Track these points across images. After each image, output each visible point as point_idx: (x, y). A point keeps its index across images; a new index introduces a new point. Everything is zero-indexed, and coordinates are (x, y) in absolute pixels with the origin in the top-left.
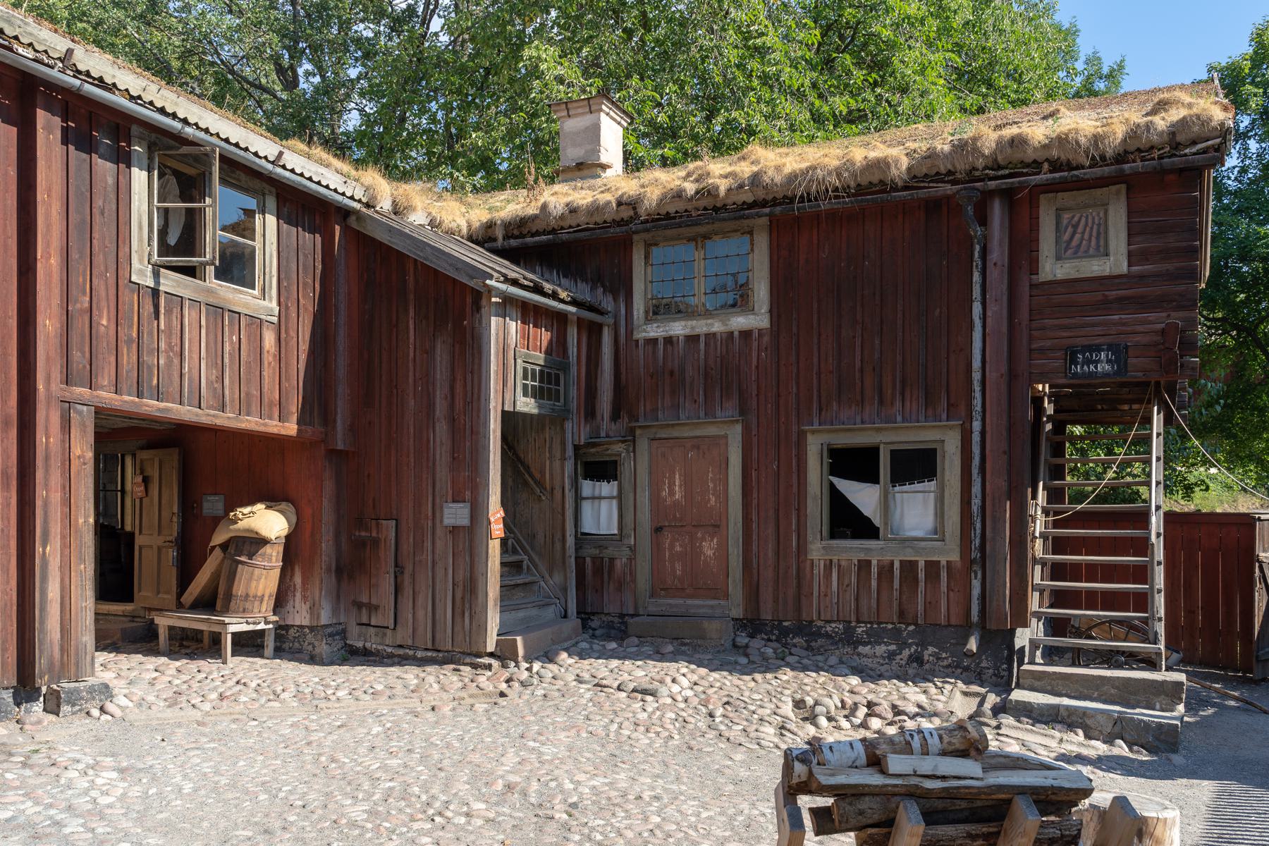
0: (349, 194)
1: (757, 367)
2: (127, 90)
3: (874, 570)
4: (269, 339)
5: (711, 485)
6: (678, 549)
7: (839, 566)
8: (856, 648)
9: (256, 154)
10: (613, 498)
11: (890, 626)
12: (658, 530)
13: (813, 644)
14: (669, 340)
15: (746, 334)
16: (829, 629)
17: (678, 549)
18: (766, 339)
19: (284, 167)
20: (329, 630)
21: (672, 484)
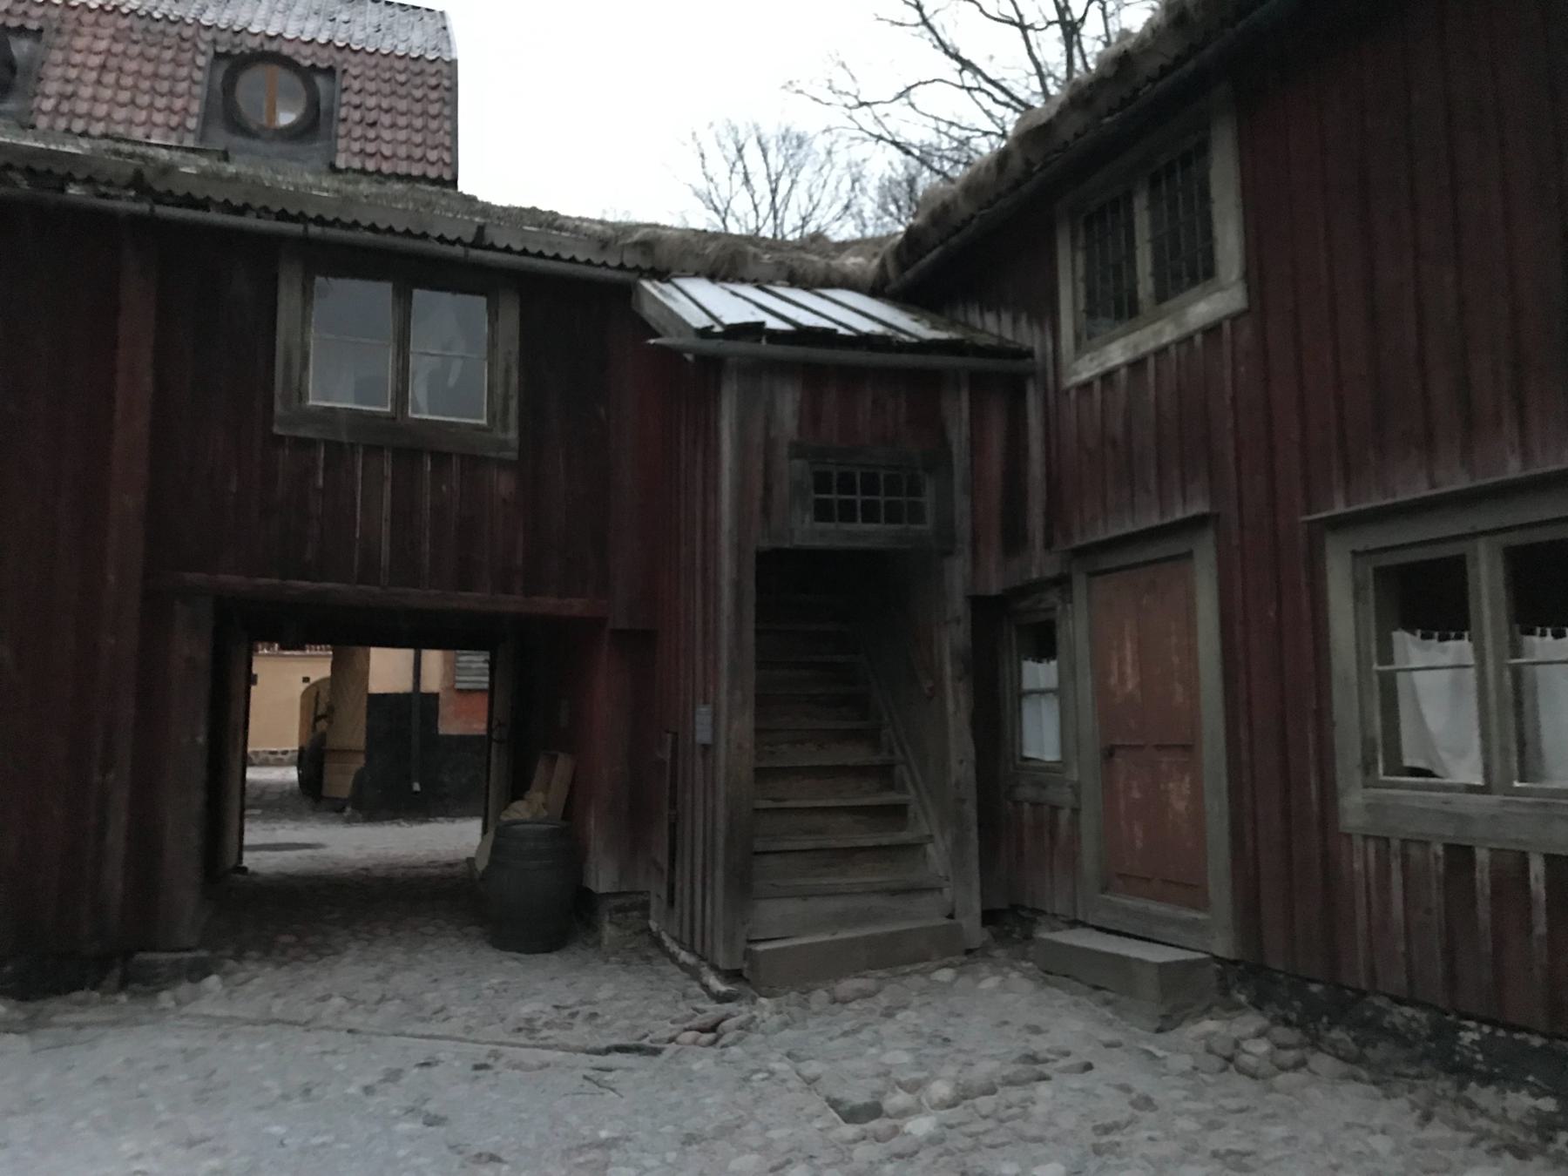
0: (614, 262)
1: (1234, 399)
2: (227, 201)
3: (1483, 877)
4: (504, 484)
5: (1176, 660)
6: (1136, 795)
7: (1405, 857)
8: (1462, 1086)
9: (441, 239)
10: (1031, 692)
11: (1537, 1042)
12: (1109, 753)
13: (1369, 1052)
14: (1108, 377)
15: (1212, 331)
16: (1398, 1020)
17: (1136, 795)
18: (1246, 332)
19: (492, 247)
20: (617, 902)
21: (1122, 662)
